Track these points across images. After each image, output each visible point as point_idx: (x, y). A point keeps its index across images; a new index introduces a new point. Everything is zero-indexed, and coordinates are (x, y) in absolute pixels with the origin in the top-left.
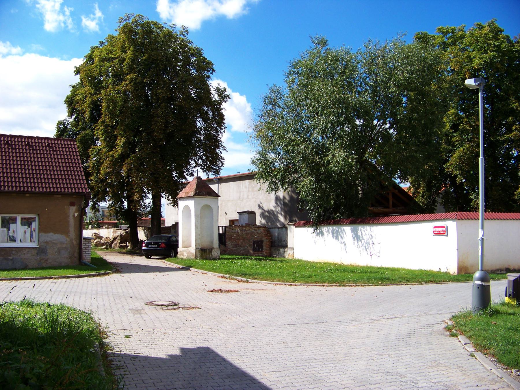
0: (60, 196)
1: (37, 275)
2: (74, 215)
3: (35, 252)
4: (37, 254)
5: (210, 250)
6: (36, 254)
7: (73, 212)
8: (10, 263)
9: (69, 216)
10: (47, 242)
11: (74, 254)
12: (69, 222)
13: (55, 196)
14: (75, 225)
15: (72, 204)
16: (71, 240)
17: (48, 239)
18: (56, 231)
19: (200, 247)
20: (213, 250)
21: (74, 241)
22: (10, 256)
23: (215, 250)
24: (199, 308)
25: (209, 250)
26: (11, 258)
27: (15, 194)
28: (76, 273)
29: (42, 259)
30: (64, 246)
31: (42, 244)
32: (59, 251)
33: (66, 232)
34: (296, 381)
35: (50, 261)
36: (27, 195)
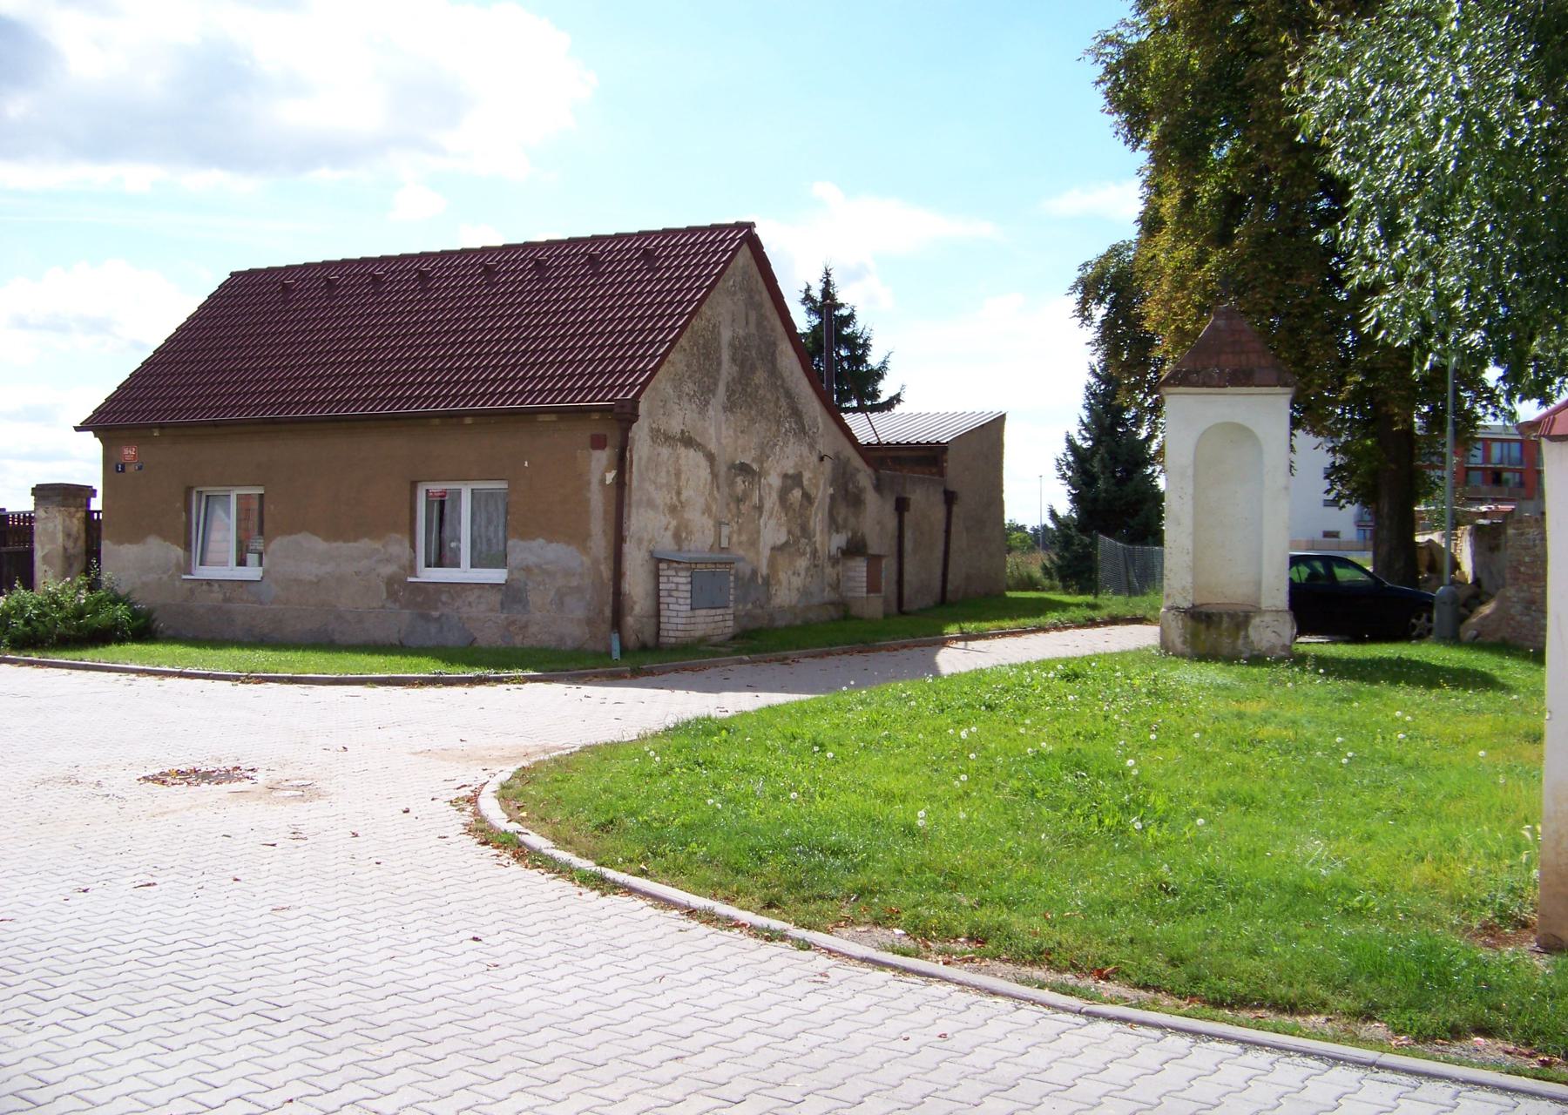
0: (553, 417)
1: (182, 657)
2: (603, 480)
3: (496, 598)
4: (502, 604)
5: (1241, 619)
6: (498, 606)
7: (599, 466)
8: (433, 629)
9: (589, 483)
10: (527, 569)
11: (601, 612)
12: (588, 501)
13: (541, 418)
14: (606, 512)
15: (598, 443)
16: (596, 562)
17: (532, 560)
18: (551, 534)
19: (1186, 605)
20: (1256, 621)
21: (602, 567)
22: (436, 609)
23: (1267, 618)
24: (154, 779)
25: (1232, 616)
26: (436, 614)
27: (437, 421)
28: (429, 667)
29: (514, 622)
30: (574, 583)
31: (517, 575)
32: (561, 597)
33: (578, 537)
34: (98, 1065)
35: (534, 629)
36: (468, 420)
